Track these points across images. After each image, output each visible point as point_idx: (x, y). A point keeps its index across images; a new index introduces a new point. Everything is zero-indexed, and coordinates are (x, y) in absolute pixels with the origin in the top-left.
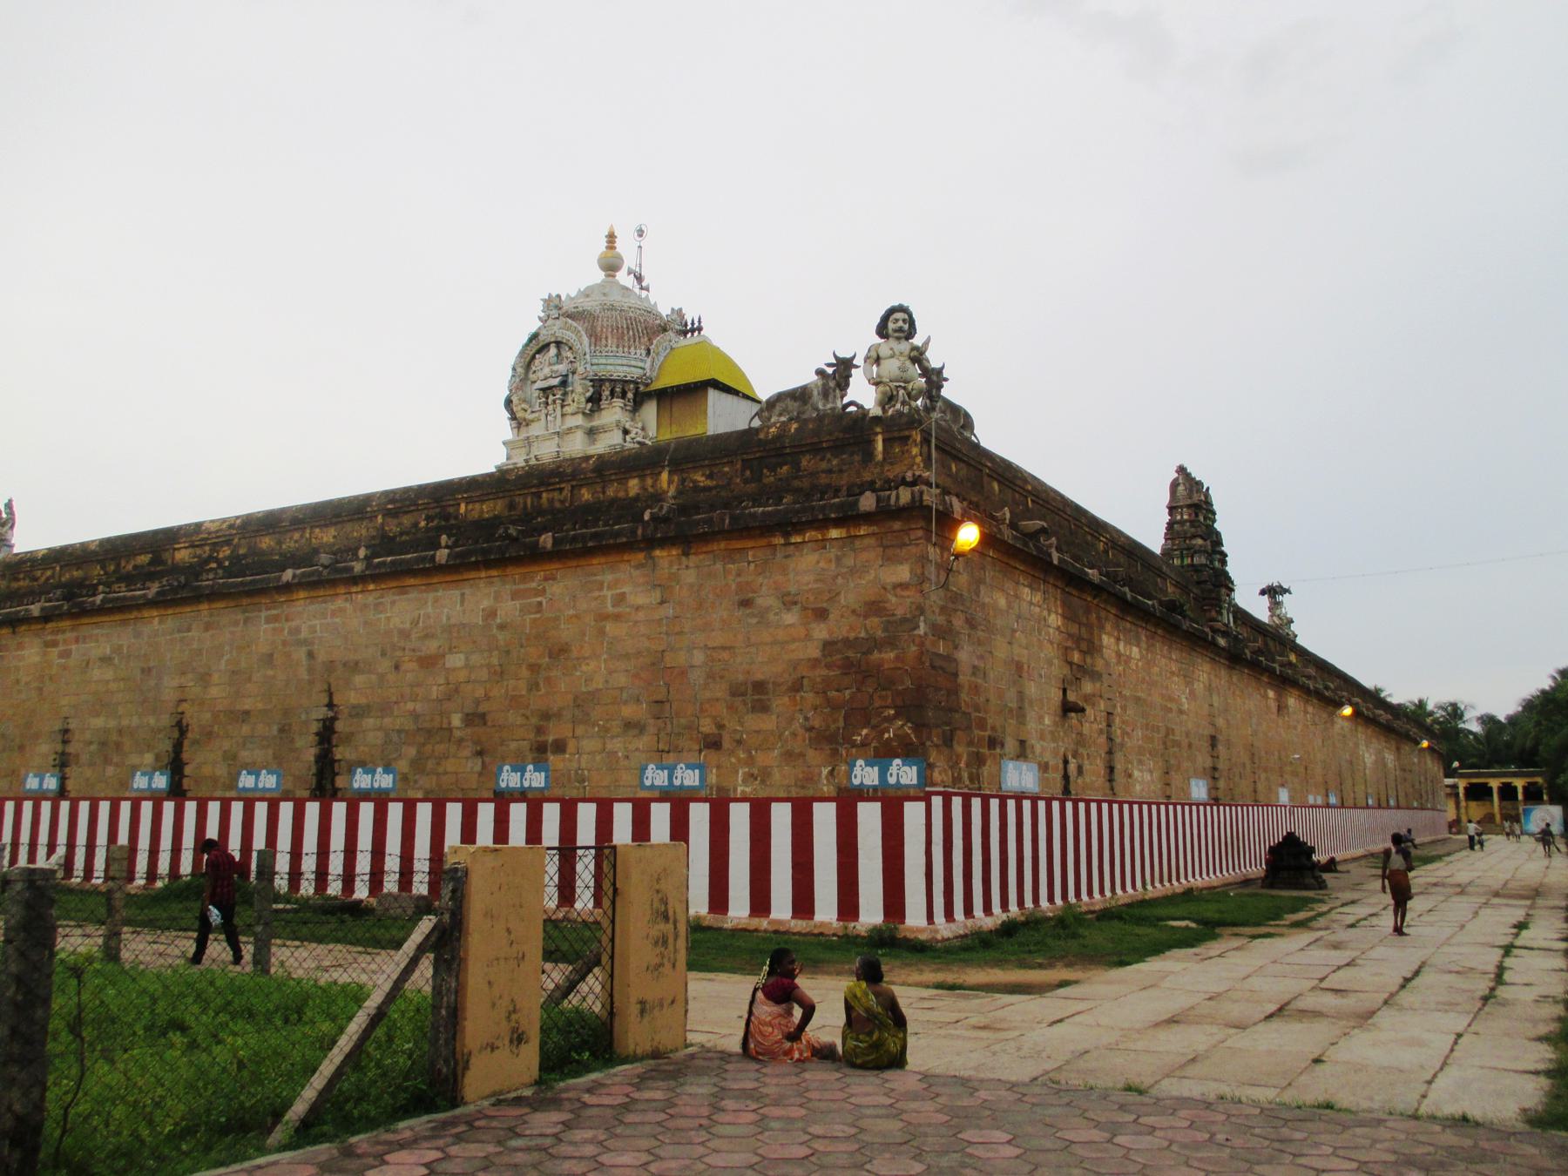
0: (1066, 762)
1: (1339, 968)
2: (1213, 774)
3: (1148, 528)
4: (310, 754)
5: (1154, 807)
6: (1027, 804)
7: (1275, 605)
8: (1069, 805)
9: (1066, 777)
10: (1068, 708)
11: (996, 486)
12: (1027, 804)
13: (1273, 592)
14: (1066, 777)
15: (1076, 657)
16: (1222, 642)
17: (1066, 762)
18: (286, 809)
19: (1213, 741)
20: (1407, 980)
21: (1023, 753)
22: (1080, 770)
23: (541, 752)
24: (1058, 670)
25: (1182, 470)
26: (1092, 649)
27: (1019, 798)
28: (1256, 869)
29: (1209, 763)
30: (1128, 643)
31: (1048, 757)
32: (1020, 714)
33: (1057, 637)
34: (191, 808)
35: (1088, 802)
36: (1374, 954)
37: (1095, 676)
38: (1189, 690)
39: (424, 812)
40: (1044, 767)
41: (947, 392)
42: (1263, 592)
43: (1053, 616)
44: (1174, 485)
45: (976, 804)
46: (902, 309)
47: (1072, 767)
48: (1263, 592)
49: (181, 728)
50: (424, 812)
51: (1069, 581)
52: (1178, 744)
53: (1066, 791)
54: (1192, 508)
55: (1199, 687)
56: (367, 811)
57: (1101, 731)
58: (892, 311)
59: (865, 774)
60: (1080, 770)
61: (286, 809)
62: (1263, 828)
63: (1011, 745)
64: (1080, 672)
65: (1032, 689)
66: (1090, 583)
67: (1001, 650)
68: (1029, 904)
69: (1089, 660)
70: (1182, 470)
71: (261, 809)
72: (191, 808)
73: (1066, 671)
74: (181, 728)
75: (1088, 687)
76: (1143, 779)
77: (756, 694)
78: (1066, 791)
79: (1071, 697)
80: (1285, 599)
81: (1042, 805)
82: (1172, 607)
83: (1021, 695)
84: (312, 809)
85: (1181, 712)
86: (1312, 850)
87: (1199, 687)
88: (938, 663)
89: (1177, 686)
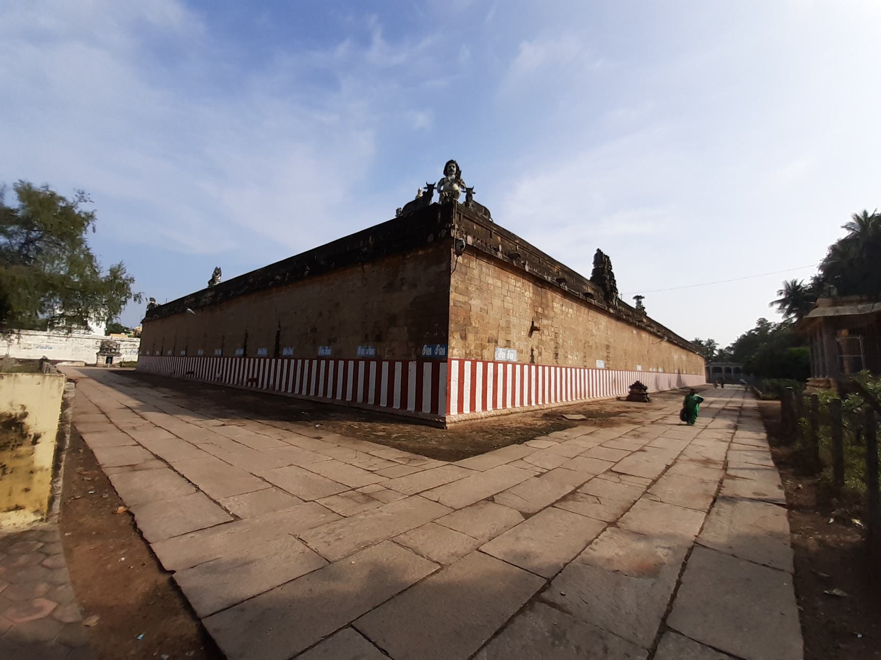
0: (532, 350)
1: (633, 452)
2: (607, 359)
3: (586, 270)
4: (274, 343)
5: (573, 370)
6: (509, 366)
7: (639, 303)
8: (533, 368)
9: (532, 356)
10: (533, 329)
11: (499, 238)
12: (509, 366)
13: (638, 298)
14: (532, 356)
15: (540, 310)
16: (612, 311)
17: (532, 350)
18: (268, 360)
19: (608, 347)
20: (668, 467)
21: (508, 344)
22: (540, 354)
23: (330, 342)
24: (529, 314)
25: (598, 250)
26: (545, 306)
27: (505, 364)
28: (625, 392)
29: (606, 354)
30: (567, 307)
31: (522, 347)
32: (508, 329)
33: (530, 301)
34: (247, 360)
35: (544, 367)
36: (656, 443)
37: (546, 317)
38: (601, 326)
39: (300, 362)
40: (520, 352)
41: (475, 198)
42: (635, 298)
43: (527, 293)
44: (596, 255)
45: (480, 365)
46: (452, 162)
47: (536, 353)
48: (635, 298)
49: (247, 335)
50: (300, 362)
51: (538, 281)
52: (591, 347)
53: (532, 362)
54: (602, 261)
55: (602, 327)
56: (286, 361)
57: (551, 340)
58: (448, 164)
59: (427, 351)
60: (540, 354)
61: (268, 360)
62: (628, 379)
63: (501, 342)
64: (538, 316)
65: (514, 320)
66: (549, 283)
67: (497, 302)
68: (540, 403)
69: (546, 312)
70: (598, 250)
71: (262, 360)
72: (247, 360)
73: (534, 315)
74: (247, 335)
75: (545, 322)
76: (573, 358)
77: (393, 320)
78: (532, 362)
79: (536, 324)
80: (642, 300)
81: (518, 367)
82: (588, 295)
83: (508, 322)
84: (274, 360)
85: (592, 335)
86: (646, 388)
87: (602, 327)
88: (458, 304)
89: (592, 326)
